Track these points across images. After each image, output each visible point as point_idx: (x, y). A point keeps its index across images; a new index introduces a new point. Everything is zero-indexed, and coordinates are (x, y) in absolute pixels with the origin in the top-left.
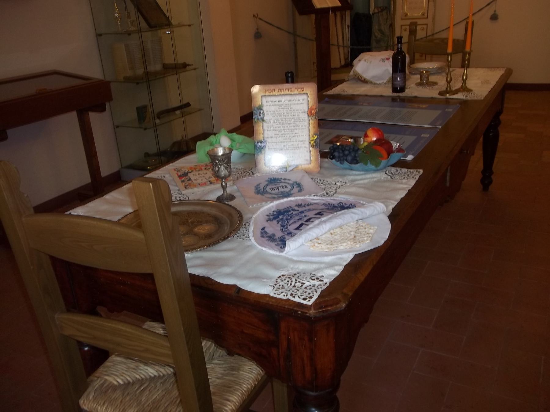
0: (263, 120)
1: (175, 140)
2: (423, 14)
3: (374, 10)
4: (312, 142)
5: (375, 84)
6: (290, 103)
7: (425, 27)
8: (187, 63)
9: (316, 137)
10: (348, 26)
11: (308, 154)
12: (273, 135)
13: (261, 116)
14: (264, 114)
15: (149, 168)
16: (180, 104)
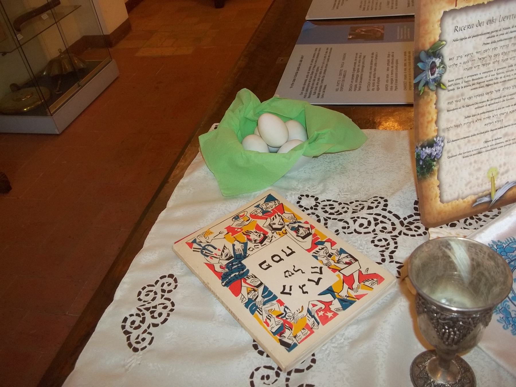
0: (439, 84)
1: (49, 59)
12: (462, 120)
13: (435, 75)
15: (25, 109)
16: (47, 2)
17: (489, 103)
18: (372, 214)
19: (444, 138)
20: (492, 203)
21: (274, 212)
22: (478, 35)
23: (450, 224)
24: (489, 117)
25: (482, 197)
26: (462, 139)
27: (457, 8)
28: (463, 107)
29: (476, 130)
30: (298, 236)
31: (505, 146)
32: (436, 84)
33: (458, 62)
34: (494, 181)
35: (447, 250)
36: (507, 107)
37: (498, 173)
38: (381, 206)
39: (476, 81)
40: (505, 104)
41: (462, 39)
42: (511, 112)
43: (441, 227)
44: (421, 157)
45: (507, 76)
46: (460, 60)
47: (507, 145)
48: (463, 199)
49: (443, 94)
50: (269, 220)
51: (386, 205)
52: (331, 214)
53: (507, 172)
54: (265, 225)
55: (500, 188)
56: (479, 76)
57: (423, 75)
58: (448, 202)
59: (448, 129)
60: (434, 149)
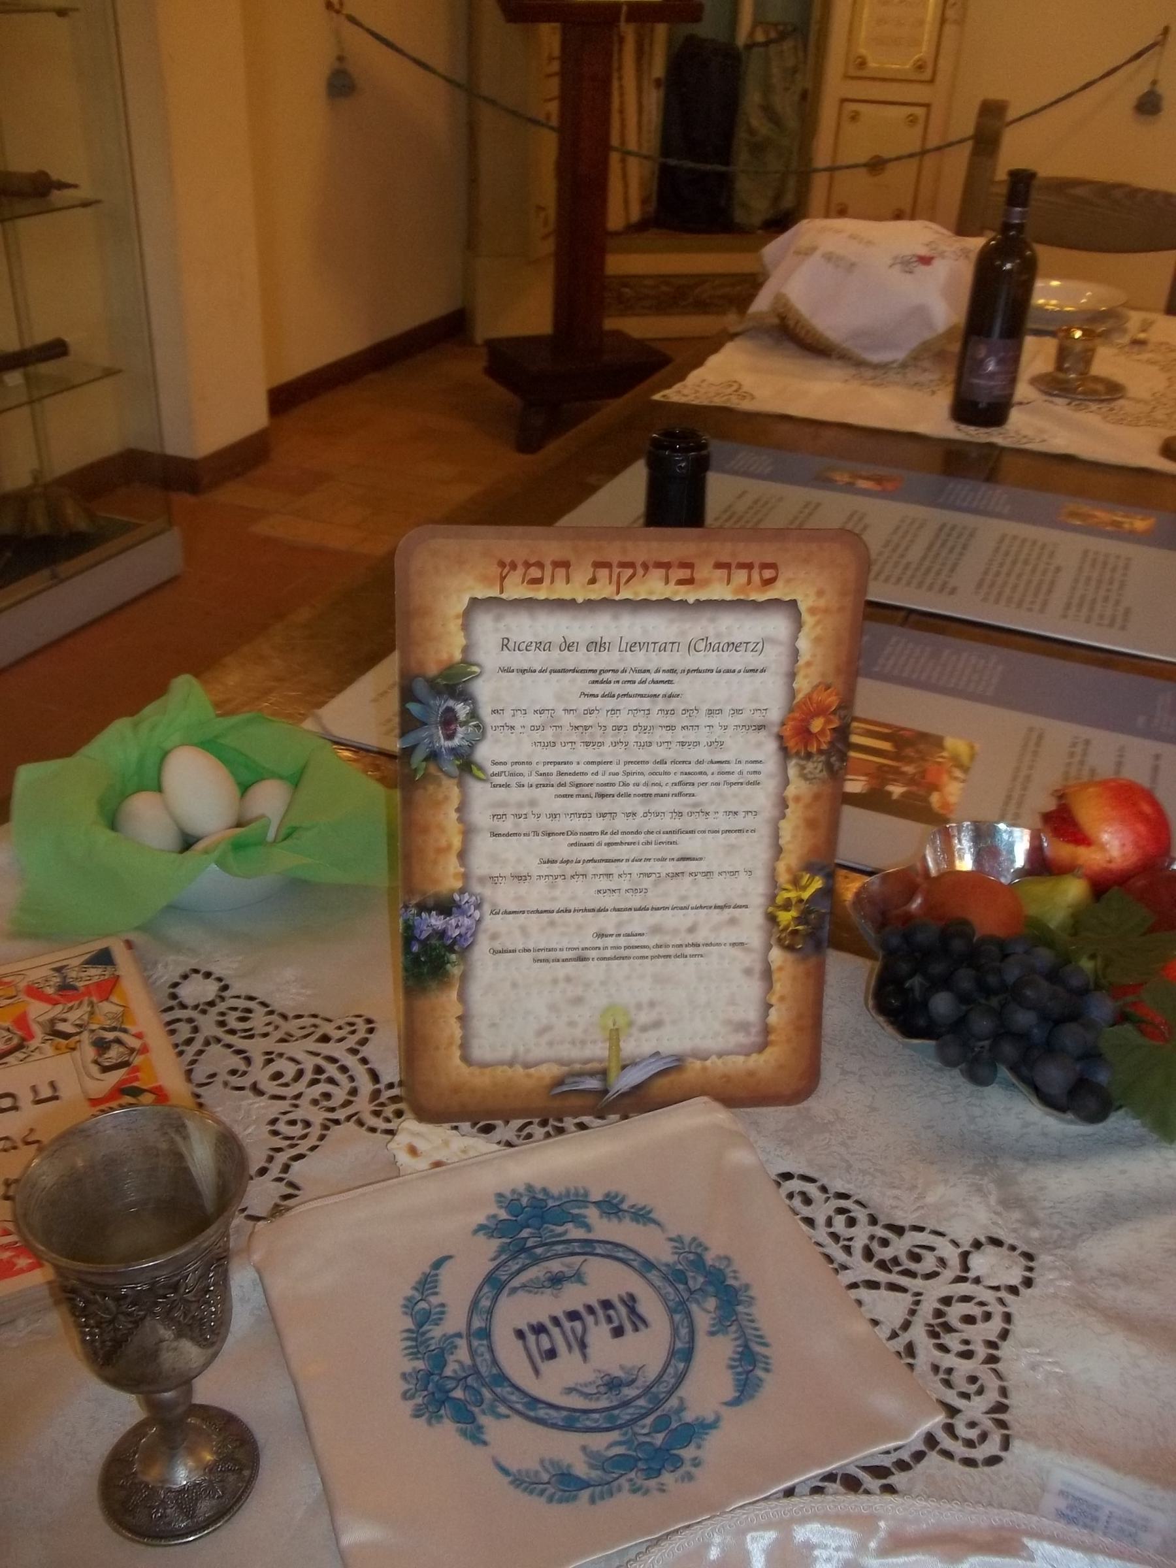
0: (467, 765)
2: (920, 67)
3: (752, 34)
4: (785, 917)
5: (860, 364)
6: (667, 660)
7: (920, 112)
8: (55, 175)
9: (818, 883)
10: (658, 83)
11: (752, 989)
12: (534, 867)
13: (456, 742)
14: (481, 728)
17: (607, 839)
18: (318, 1055)
19: (481, 899)
20: (607, 1096)
21: (88, 991)
22: (564, 671)
23: (481, 1124)
24: (609, 875)
25: (581, 1074)
26: (533, 912)
27: (504, 596)
28: (536, 834)
29: (573, 898)
30: (96, 1062)
31: (653, 957)
32: (458, 763)
33: (518, 721)
34: (618, 1040)
35: (178, 1139)
36: (659, 860)
37: (631, 1024)
38: (352, 1041)
39: (568, 779)
40: (652, 851)
41: (523, 671)
42: (670, 875)
43: (456, 1128)
44: (417, 933)
45: (653, 784)
46: (518, 721)
47: (659, 956)
48: (527, 1066)
49: (481, 795)
50: (59, 1008)
51: (363, 1042)
52: (232, 1032)
53: (657, 1024)
54: (40, 1019)
55: (634, 1064)
56: (578, 769)
57: (423, 733)
58: (484, 1065)
59: (494, 880)
60: (453, 921)
